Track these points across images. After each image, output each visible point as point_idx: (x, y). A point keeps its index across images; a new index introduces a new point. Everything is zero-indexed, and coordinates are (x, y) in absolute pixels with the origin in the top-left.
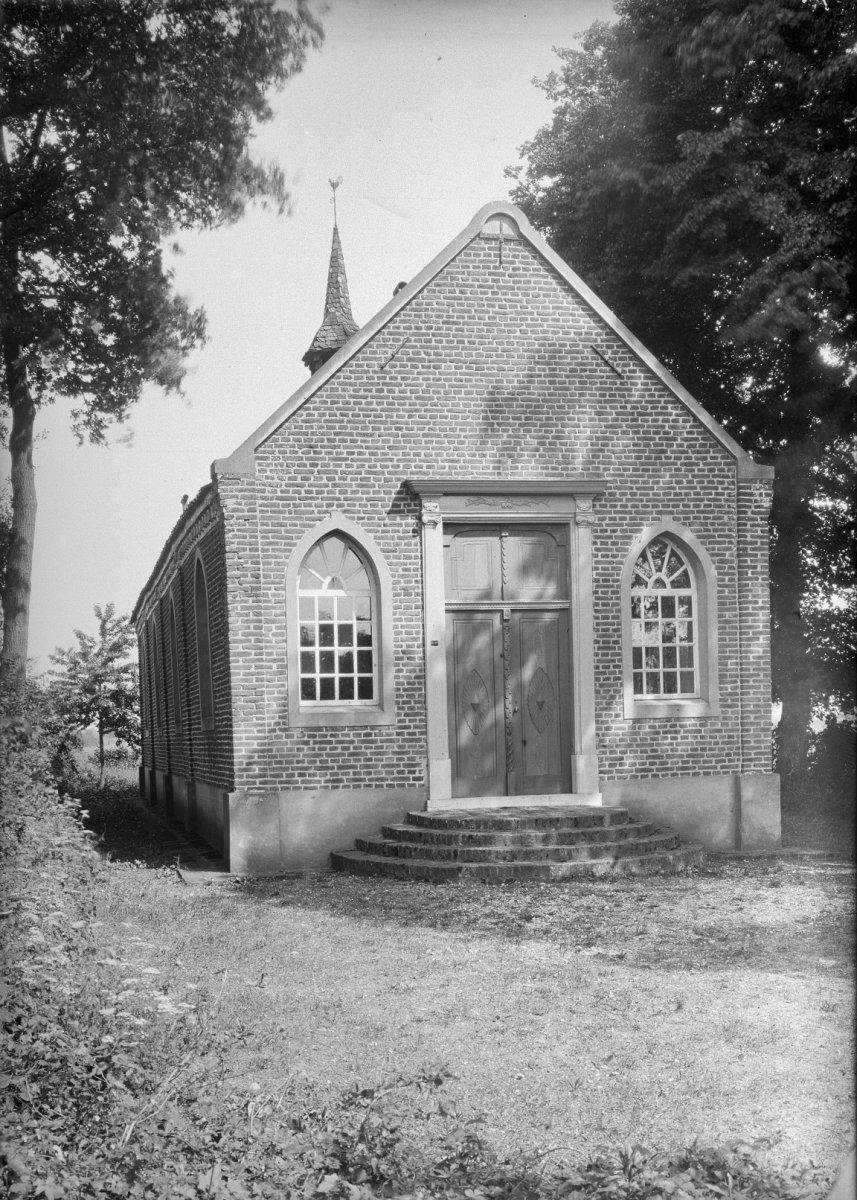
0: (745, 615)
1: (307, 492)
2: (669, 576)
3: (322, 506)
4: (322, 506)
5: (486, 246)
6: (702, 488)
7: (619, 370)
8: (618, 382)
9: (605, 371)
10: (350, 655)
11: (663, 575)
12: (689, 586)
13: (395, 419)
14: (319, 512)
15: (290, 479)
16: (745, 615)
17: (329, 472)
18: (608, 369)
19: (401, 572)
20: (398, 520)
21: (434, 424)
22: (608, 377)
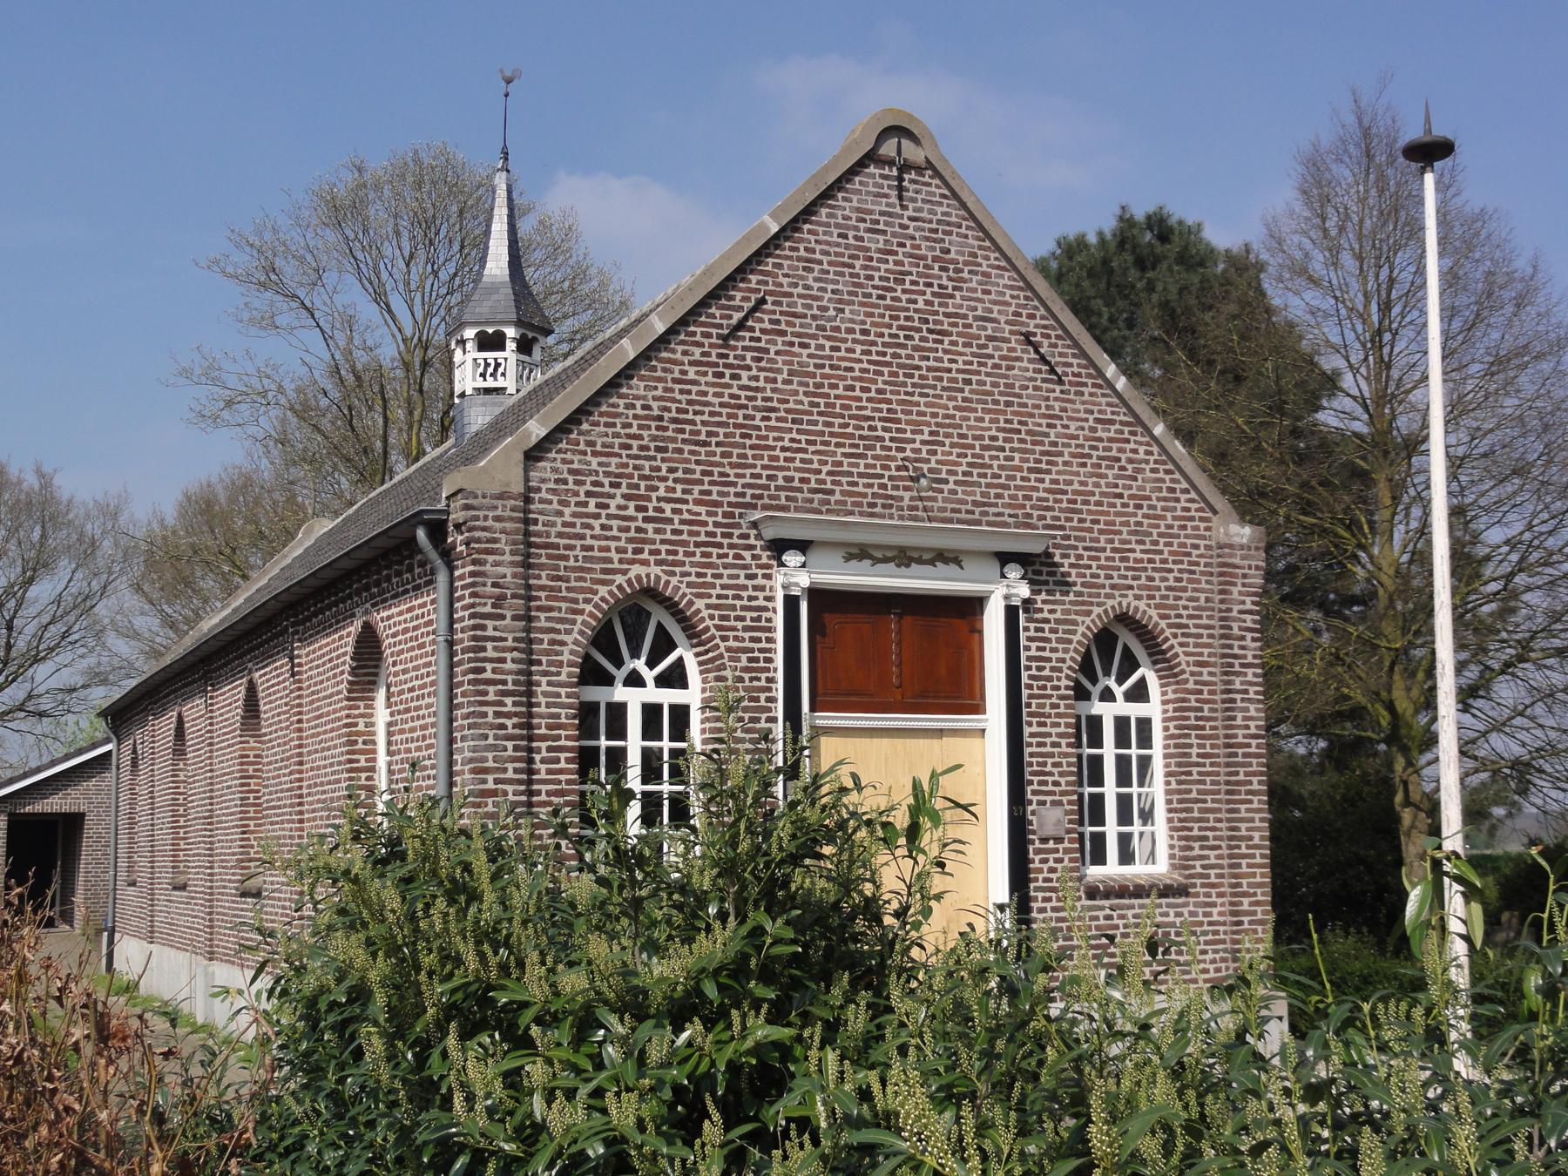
0: (521, 738)
1: (603, 527)
2: (1120, 682)
3: (625, 551)
4: (625, 551)
5: (877, 171)
6: (1171, 553)
7: (1059, 370)
8: (1058, 388)
9: (1040, 371)
10: (1141, 784)
11: (640, 665)
12: (684, 686)
13: (741, 420)
14: (621, 561)
15: (578, 504)
16: (521, 738)
17: (639, 498)
18: (1044, 368)
19: (744, 663)
20: (1058, 597)
21: (661, 418)
22: (1044, 380)
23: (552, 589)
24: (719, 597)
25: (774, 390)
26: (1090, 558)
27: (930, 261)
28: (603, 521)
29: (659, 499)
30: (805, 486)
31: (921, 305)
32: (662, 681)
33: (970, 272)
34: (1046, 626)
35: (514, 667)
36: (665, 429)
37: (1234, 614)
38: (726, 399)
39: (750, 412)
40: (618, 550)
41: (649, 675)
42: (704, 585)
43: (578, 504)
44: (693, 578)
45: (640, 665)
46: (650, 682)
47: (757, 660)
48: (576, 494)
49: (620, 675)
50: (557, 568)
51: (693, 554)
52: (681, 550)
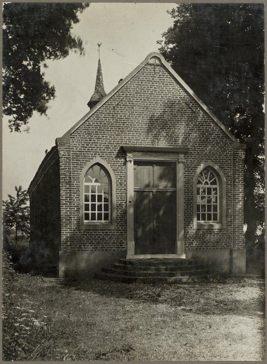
2: (209, 181)
10: (101, 205)
13: (118, 125)
14: (92, 156)
15: (82, 145)
19: (119, 177)
20: (118, 160)
21: (100, 126)
23: (77, 163)
24: (113, 163)
25: (126, 118)
26: (201, 153)
27: (163, 87)
28: (88, 148)
29: (100, 143)
30: (133, 139)
31: (160, 97)
32: (212, 184)
33: (172, 89)
34: (190, 168)
35: (68, 179)
36: (101, 128)
37: (237, 165)
38: (115, 121)
39: (120, 123)
40: (91, 154)
41: (209, 182)
42: (110, 161)
43: (82, 145)
44: (107, 160)
45: (208, 180)
46: (209, 184)
47: (122, 177)
48: (82, 143)
49: (203, 182)
50: (78, 158)
51: (107, 155)
52: (105, 154)
